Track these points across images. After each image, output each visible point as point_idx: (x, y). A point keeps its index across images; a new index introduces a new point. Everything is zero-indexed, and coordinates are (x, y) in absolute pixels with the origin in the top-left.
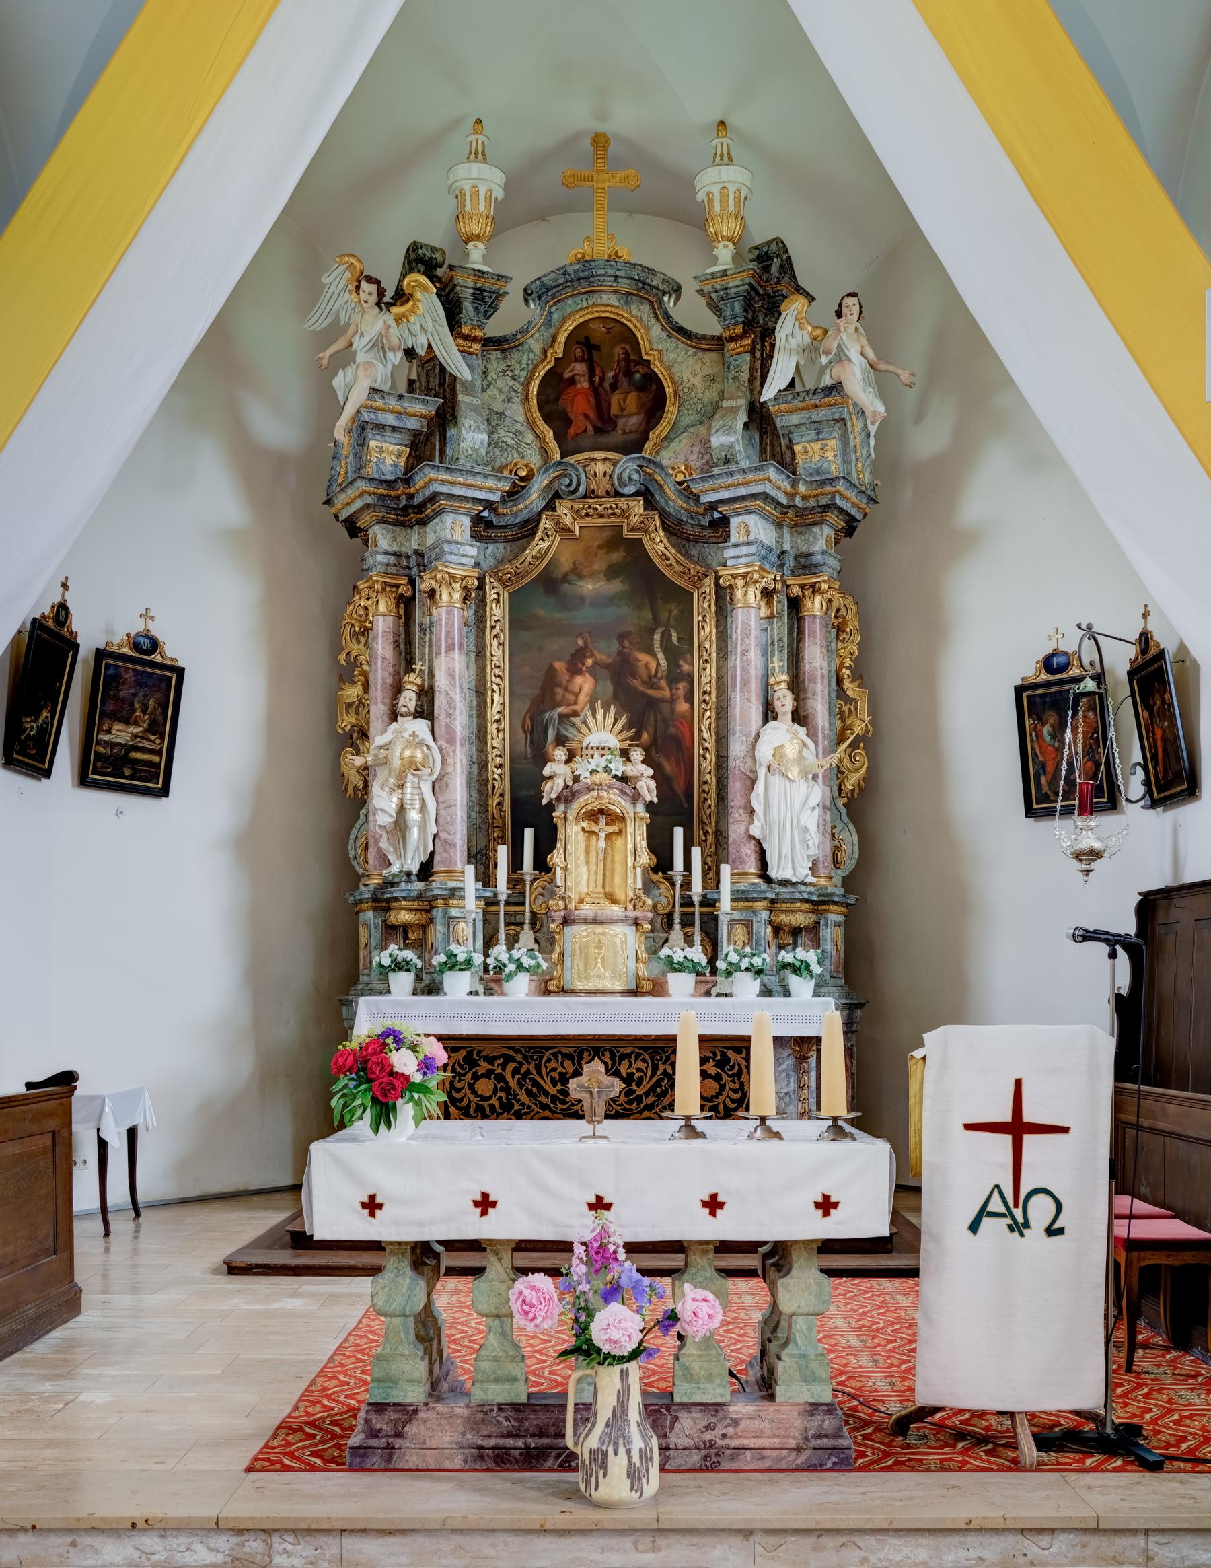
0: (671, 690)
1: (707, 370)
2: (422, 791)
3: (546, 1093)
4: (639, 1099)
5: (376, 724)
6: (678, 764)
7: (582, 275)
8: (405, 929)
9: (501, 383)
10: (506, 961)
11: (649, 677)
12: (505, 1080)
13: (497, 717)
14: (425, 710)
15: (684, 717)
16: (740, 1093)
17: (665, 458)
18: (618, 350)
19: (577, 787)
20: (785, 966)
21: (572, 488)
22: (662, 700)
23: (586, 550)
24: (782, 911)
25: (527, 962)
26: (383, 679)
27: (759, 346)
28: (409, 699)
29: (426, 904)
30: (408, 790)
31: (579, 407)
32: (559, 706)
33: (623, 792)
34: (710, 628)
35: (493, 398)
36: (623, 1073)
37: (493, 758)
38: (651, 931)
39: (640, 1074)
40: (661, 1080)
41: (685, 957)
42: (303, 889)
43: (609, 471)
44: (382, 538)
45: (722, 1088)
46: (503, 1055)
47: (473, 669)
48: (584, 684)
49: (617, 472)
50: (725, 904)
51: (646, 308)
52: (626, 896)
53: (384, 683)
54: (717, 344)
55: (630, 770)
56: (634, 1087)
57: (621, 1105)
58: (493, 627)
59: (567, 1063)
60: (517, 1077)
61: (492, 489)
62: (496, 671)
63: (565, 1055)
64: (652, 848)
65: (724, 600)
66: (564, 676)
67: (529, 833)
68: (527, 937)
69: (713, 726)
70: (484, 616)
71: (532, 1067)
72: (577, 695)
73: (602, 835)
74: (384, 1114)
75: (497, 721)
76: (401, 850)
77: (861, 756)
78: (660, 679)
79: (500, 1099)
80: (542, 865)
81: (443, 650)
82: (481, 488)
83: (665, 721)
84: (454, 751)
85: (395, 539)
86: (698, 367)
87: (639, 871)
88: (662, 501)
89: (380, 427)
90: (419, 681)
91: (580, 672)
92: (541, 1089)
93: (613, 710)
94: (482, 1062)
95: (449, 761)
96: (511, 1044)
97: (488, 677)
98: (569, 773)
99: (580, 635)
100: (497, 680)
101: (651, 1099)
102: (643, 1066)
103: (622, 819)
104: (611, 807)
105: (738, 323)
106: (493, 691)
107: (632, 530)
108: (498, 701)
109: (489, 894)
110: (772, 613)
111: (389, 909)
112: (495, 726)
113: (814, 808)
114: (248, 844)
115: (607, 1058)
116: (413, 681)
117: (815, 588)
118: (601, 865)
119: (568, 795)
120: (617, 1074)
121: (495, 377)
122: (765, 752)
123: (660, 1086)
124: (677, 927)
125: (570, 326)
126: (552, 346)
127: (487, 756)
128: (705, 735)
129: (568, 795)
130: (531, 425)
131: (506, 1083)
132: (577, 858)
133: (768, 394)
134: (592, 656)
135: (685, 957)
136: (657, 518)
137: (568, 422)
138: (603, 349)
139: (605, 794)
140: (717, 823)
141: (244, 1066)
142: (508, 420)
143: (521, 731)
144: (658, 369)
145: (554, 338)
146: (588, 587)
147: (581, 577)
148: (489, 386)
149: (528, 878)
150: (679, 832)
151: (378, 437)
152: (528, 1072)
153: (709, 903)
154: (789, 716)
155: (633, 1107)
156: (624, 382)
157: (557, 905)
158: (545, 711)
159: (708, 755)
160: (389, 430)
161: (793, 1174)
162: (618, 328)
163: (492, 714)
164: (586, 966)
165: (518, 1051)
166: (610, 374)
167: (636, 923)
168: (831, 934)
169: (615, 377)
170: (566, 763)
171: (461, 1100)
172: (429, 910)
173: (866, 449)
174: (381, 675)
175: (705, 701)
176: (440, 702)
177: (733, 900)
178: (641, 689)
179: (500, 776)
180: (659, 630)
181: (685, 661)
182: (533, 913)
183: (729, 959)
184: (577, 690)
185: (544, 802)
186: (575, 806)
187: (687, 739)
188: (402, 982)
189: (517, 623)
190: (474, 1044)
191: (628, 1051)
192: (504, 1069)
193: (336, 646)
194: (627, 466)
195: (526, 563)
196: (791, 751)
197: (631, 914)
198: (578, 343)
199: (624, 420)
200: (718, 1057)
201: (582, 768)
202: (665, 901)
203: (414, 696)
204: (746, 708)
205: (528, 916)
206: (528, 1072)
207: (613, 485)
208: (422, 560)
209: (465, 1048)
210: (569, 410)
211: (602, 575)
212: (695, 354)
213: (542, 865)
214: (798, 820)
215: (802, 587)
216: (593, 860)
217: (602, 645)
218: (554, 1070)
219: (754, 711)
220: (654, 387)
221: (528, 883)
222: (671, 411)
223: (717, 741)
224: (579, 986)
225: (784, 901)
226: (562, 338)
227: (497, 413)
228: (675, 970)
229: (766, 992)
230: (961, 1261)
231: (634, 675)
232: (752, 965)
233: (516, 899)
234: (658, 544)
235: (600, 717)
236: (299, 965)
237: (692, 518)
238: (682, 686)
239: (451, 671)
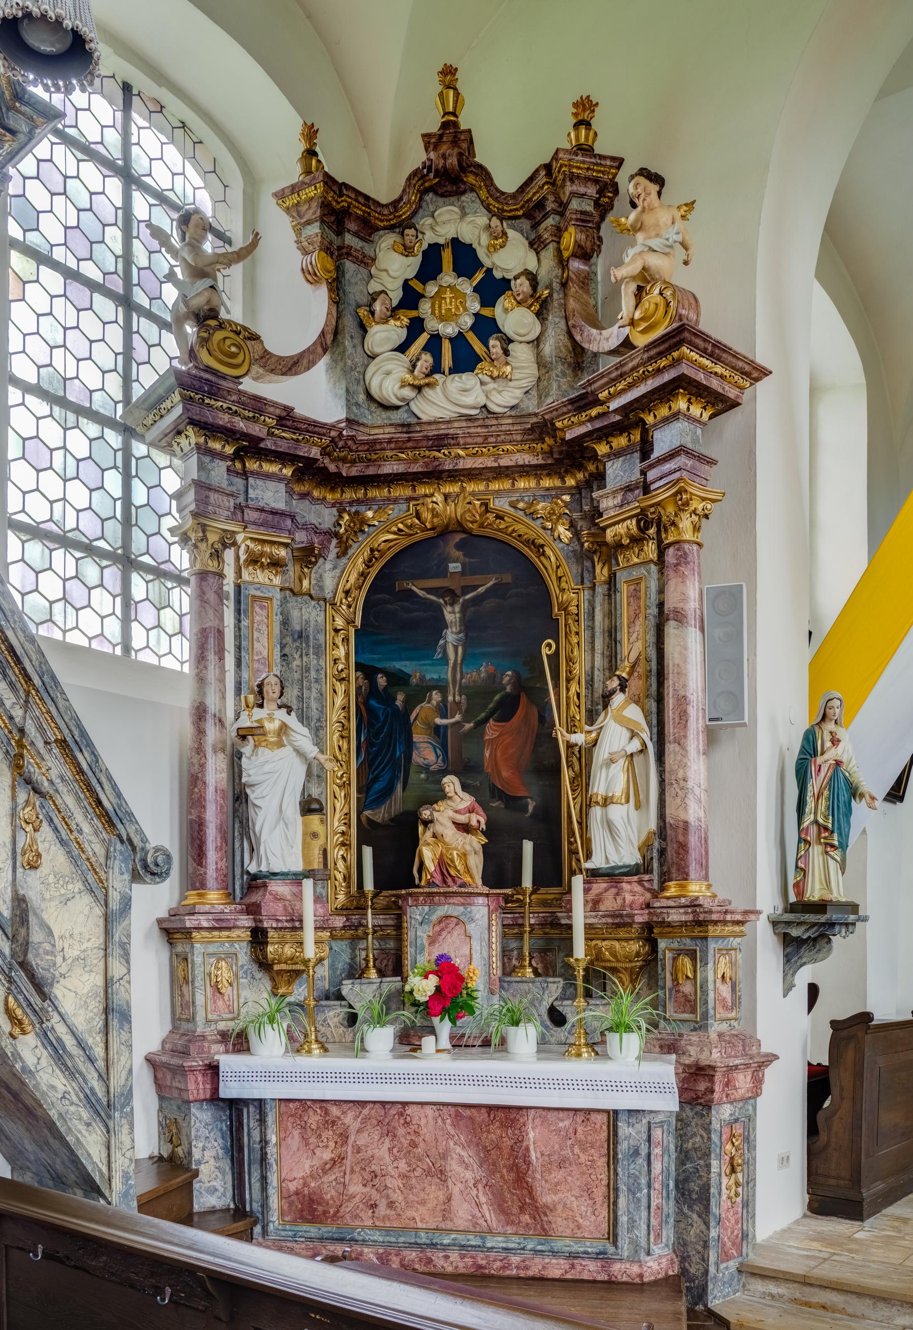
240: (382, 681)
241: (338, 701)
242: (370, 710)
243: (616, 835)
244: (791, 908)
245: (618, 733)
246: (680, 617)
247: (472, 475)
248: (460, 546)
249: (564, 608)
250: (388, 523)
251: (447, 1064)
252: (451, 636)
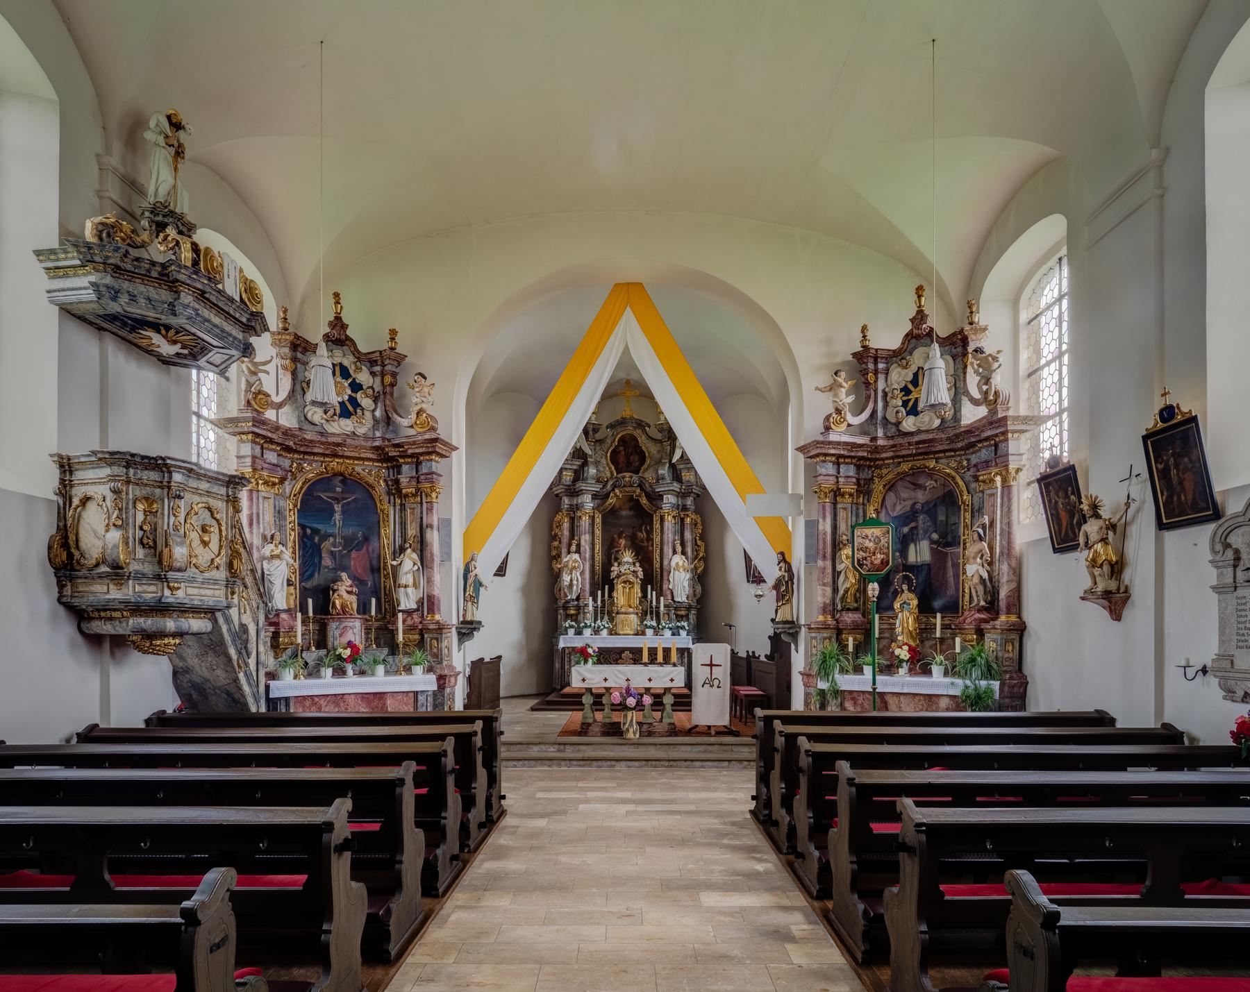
2: (576, 574)
5: (563, 554)
12: (608, 656)
17: (646, 475)
28: (573, 548)
29: (578, 608)
31: (622, 459)
42: (540, 601)
44: (566, 500)
48: (623, 542)
50: (662, 608)
54: (660, 441)
61: (597, 488)
65: (662, 519)
68: (606, 617)
74: (586, 662)
76: (571, 593)
77: (702, 563)
80: (610, 596)
108: (598, 547)
114: (526, 590)
116: (575, 542)
119: (618, 576)
122: (673, 564)
129: (618, 576)
133: (674, 461)
141: (524, 657)
146: (624, 513)
153: (658, 608)
161: (668, 677)
168: (692, 617)
174: (565, 540)
179: (599, 577)
188: (571, 632)
189: (604, 523)
193: (551, 529)
194: (635, 478)
196: (681, 564)
204: (668, 550)
208: (578, 507)
213: (610, 596)
222: (648, 461)
229: (673, 634)
230: (701, 696)
233: (603, 606)
234: (644, 501)
236: (539, 626)
239: (585, 539)
240: (309, 531)
241: (293, 536)
242: (304, 543)
243: (408, 599)
244: (462, 623)
245: (409, 562)
246: (431, 526)
247: (348, 458)
248: (341, 481)
249: (382, 511)
250: (312, 469)
251: (357, 679)
252: (337, 516)
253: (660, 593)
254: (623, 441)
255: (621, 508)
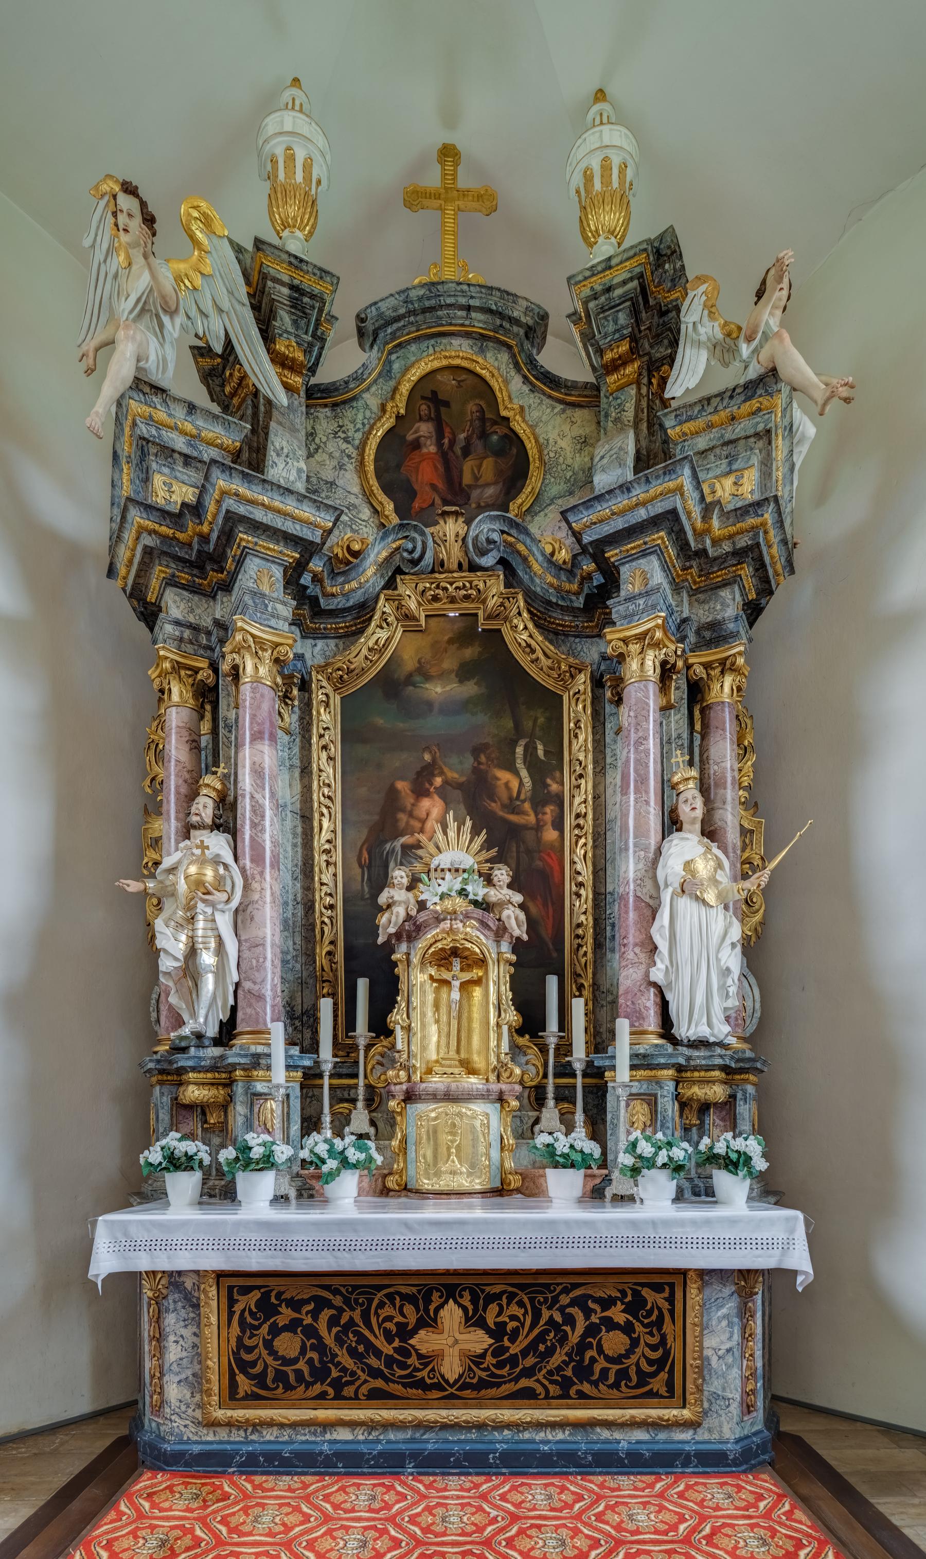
0: (536, 815)
1: (577, 431)
3: (378, 1353)
4: (513, 1361)
6: (545, 905)
7: (427, 304)
8: (201, 1109)
9: (331, 447)
10: (325, 1155)
11: (511, 798)
13: (327, 846)
14: (226, 820)
15: (551, 846)
16: (661, 1351)
18: (471, 407)
19: (422, 917)
20: (712, 1159)
21: (416, 555)
22: (525, 827)
23: (434, 645)
24: (694, 1082)
25: (353, 1155)
26: (177, 787)
27: (645, 381)
28: (205, 808)
29: (224, 1077)
30: (200, 924)
32: (402, 836)
33: (484, 924)
34: (585, 736)
35: (322, 464)
36: (490, 1322)
37: (321, 898)
38: (519, 1110)
39: (514, 1324)
40: (545, 1332)
41: (572, 1147)
43: (462, 533)
45: (635, 1343)
46: (315, 1298)
47: (298, 787)
48: (432, 806)
49: (472, 534)
50: (623, 1073)
51: (504, 357)
52: (488, 1064)
53: (178, 793)
55: (494, 895)
56: (506, 1343)
57: (487, 1369)
58: (321, 736)
59: (409, 1309)
60: (335, 1330)
62: (326, 790)
63: (405, 1298)
64: (519, 1006)
66: (408, 799)
67: (362, 985)
68: (360, 1120)
69: (590, 855)
70: (310, 724)
71: (357, 1315)
72: (423, 822)
73: (456, 984)
75: (327, 852)
78: (524, 801)
79: (310, 1362)
80: (380, 1027)
81: (248, 740)
82: (294, 518)
83: (529, 852)
84: (262, 873)
85: (192, 611)
86: (566, 428)
87: (505, 1029)
88: (526, 578)
89: (168, 452)
90: (218, 786)
91: (427, 794)
92: (370, 1346)
93: (469, 823)
94: (283, 1309)
95: (255, 885)
96: (327, 1281)
97: (315, 797)
98: (412, 901)
99: (427, 749)
100: (327, 802)
101: (530, 1361)
102: (519, 1312)
103: (482, 962)
104: (469, 945)
105: (623, 338)
106: (322, 815)
107: (489, 617)
108: (327, 827)
109: (307, 1063)
110: (669, 701)
111: (180, 1084)
112: (324, 857)
113: (733, 945)
115: (466, 1301)
117: (726, 666)
118: (454, 1023)
119: (411, 930)
120: (481, 1323)
121: (324, 439)
122: (672, 867)
123: (544, 1341)
124: (551, 1103)
125: (415, 374)
126: (393, 398)
127: (313, 893)
128: (579, 867)
129: (411, 930)
130: (368, 496)
131: (320, 1338)
132: (423, 1015)
134: (442, 773)
135: (572, 1147)
136: (520, 597)
137: (412, 494)
138: (454, 406)
139: (460, 925)
140: (594, 974)
142: (340, 492)
143: (356, 865)
144: (519, 427)
145: (395, 390)
146: (436, 690)
147: (428, 678)
148: (317, 450)
149: (362, 1043)
150: (552, 982)
151: (166, 470)
152: (351, 1322)
154: (698, 826)
155: (504, 1372)
156: (478, 445)
157: (398, 1076)
158: (386, 842)
159: (582, 892)
160: (180, 460)
162: (471, 380)
163: (320, 841)
164: (435, 1157)
165: (336, 1292)
166: (462, 436)
167: (501, 1099)
169: (468, 439)
170: (410, 888)
171: (253, 1364)
172: (229, 1084)
173: (788, 488)
175: (578, 826)
176: (245, 808)
177: (633, 1067)
178: (501, 813)
179: (332, 929)
180: (522, 742)
181: (553, 779)
182: (369, 1087)
183: (639, 1151)
184: (423, 815)
185: (380, 940)
186: (421, 944)
187: (556, 874)
188: (183, 1186)
189: (349, 736)
190: (271, 1282)
191: (497, 1289)
192: (315, 1318)
195: (362, 656)
196: (703, 868)
197: (495, 1087)
198: (423, 398)
199: (479, 491)
200: (629, 1298)
201: (429, 894)
202: (533, 1070)
203: (210, 803)
204: (638, 812)
205: (361, 1091)
206: (351, 1322)
207: (466, 553)
209: (259, 1288)
210: (413, 479)
211: (453, 676)
212: (564, 411)
214: (718, 960)
215: (707, 666)
216: (444, 1018)
217: (454, 760)
218: (389, 1319)
219: (652, 817)
220: (514, 451)
221: (361, 1048)
222: (534, 481)
223: (595, 873)
224: (427, 1184)
225: (696, 1069)
226: (405, 388)
227: (327, 483)
228: (556, 1165)
231: (492, 797)
232: (670, 1159)
233: (346, 1068)
234: (521, 633)
235: (452, 834)
237: (563, 599)
238: (549, 809)
253: (604, 1006)
254: (430, 398)
255: (423, 672)
